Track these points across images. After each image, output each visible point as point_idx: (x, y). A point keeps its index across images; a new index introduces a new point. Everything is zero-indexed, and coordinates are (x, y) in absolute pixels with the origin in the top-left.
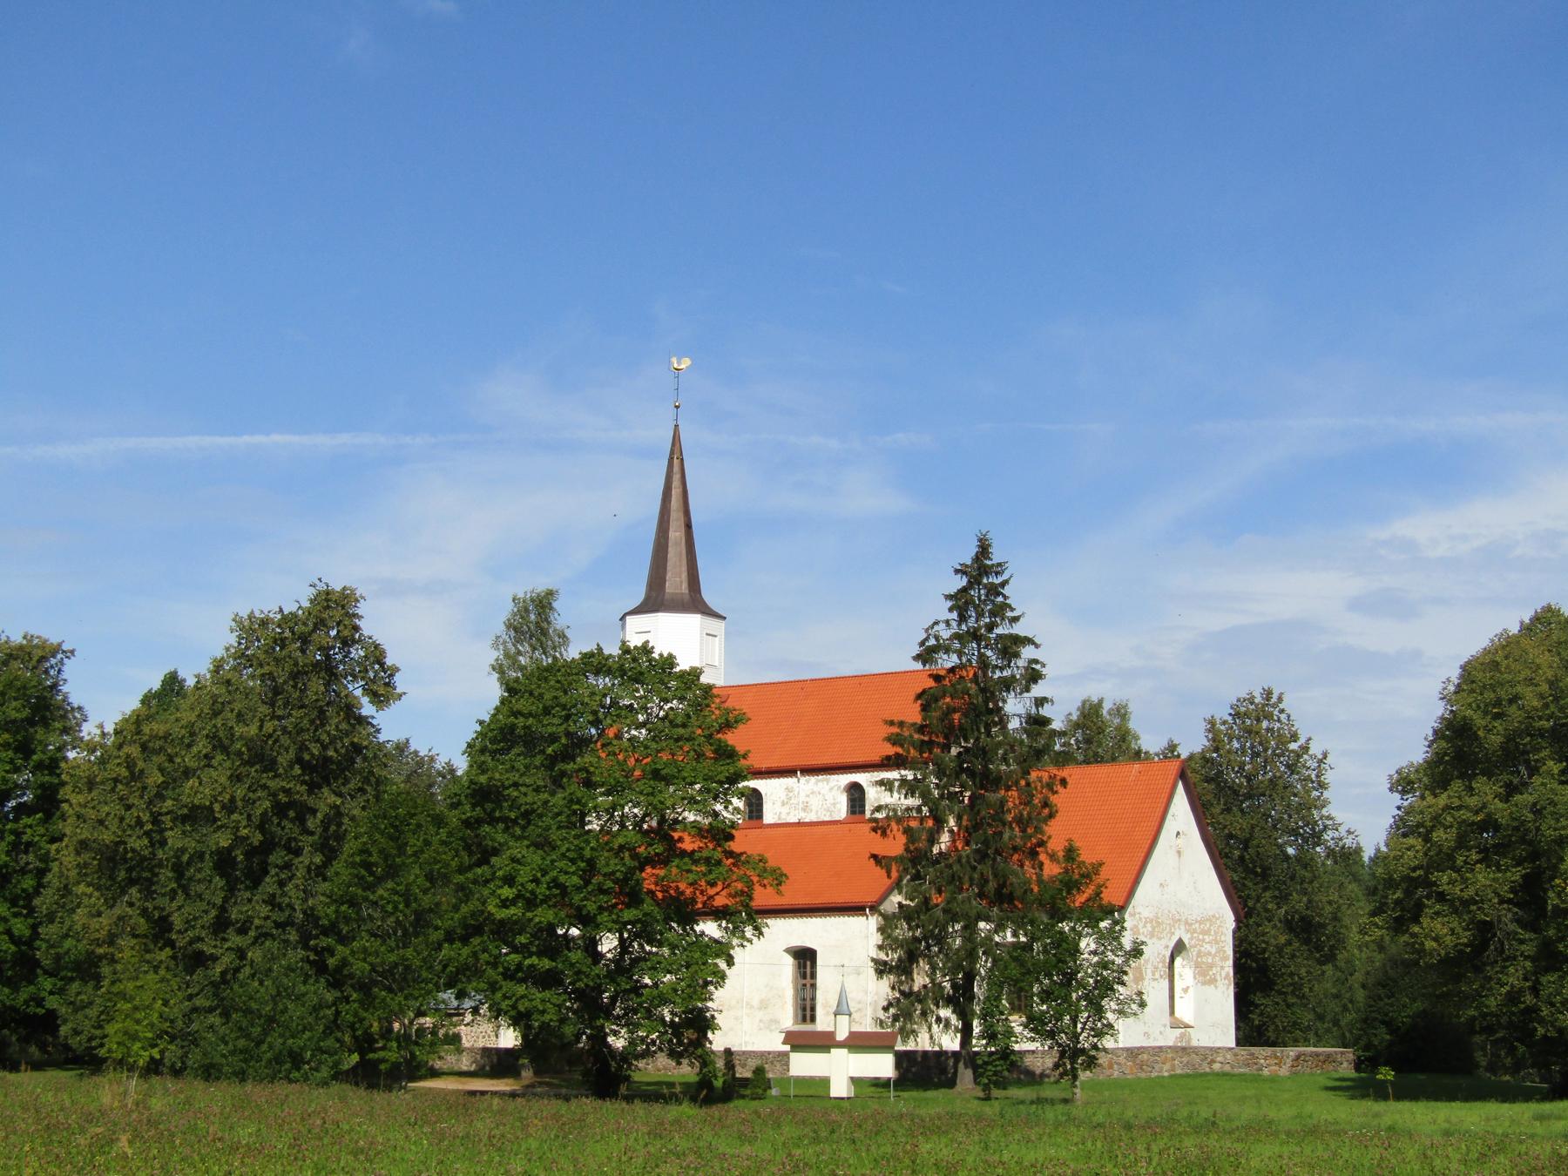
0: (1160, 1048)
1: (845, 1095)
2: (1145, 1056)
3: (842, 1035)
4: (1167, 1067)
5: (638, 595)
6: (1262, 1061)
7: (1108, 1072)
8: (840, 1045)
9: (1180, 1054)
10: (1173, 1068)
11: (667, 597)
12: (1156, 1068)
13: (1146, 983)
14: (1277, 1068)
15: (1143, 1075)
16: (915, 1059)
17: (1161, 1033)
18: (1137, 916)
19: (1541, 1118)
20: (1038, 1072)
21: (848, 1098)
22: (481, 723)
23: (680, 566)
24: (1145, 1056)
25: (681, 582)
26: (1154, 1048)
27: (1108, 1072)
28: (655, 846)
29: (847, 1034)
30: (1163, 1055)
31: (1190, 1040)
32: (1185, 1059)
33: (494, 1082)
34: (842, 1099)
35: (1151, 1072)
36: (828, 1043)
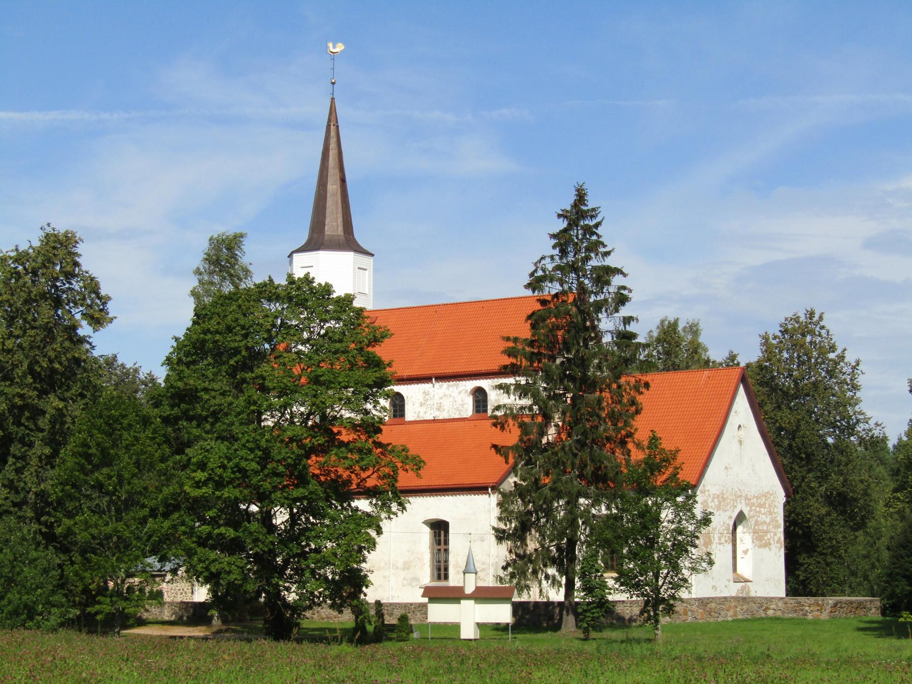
0: (725, 598)
2: (713, 605)
3: (469, 590)
4: (731, 613)
6: (807, 608)
7: (683, 618)
8: (468, 597)
10: (735, 614)
14: (818, 613)
17: (726, 586)
18: (707, 493)
20: (627, 617)
21: (475, 640)
24: (713, 605)
26: (720, 598)
27: (683, 618)
30: (727, 604)
31: (749, 592)
32: (745, 607)
34: (470, 640)
35: (718, 617)
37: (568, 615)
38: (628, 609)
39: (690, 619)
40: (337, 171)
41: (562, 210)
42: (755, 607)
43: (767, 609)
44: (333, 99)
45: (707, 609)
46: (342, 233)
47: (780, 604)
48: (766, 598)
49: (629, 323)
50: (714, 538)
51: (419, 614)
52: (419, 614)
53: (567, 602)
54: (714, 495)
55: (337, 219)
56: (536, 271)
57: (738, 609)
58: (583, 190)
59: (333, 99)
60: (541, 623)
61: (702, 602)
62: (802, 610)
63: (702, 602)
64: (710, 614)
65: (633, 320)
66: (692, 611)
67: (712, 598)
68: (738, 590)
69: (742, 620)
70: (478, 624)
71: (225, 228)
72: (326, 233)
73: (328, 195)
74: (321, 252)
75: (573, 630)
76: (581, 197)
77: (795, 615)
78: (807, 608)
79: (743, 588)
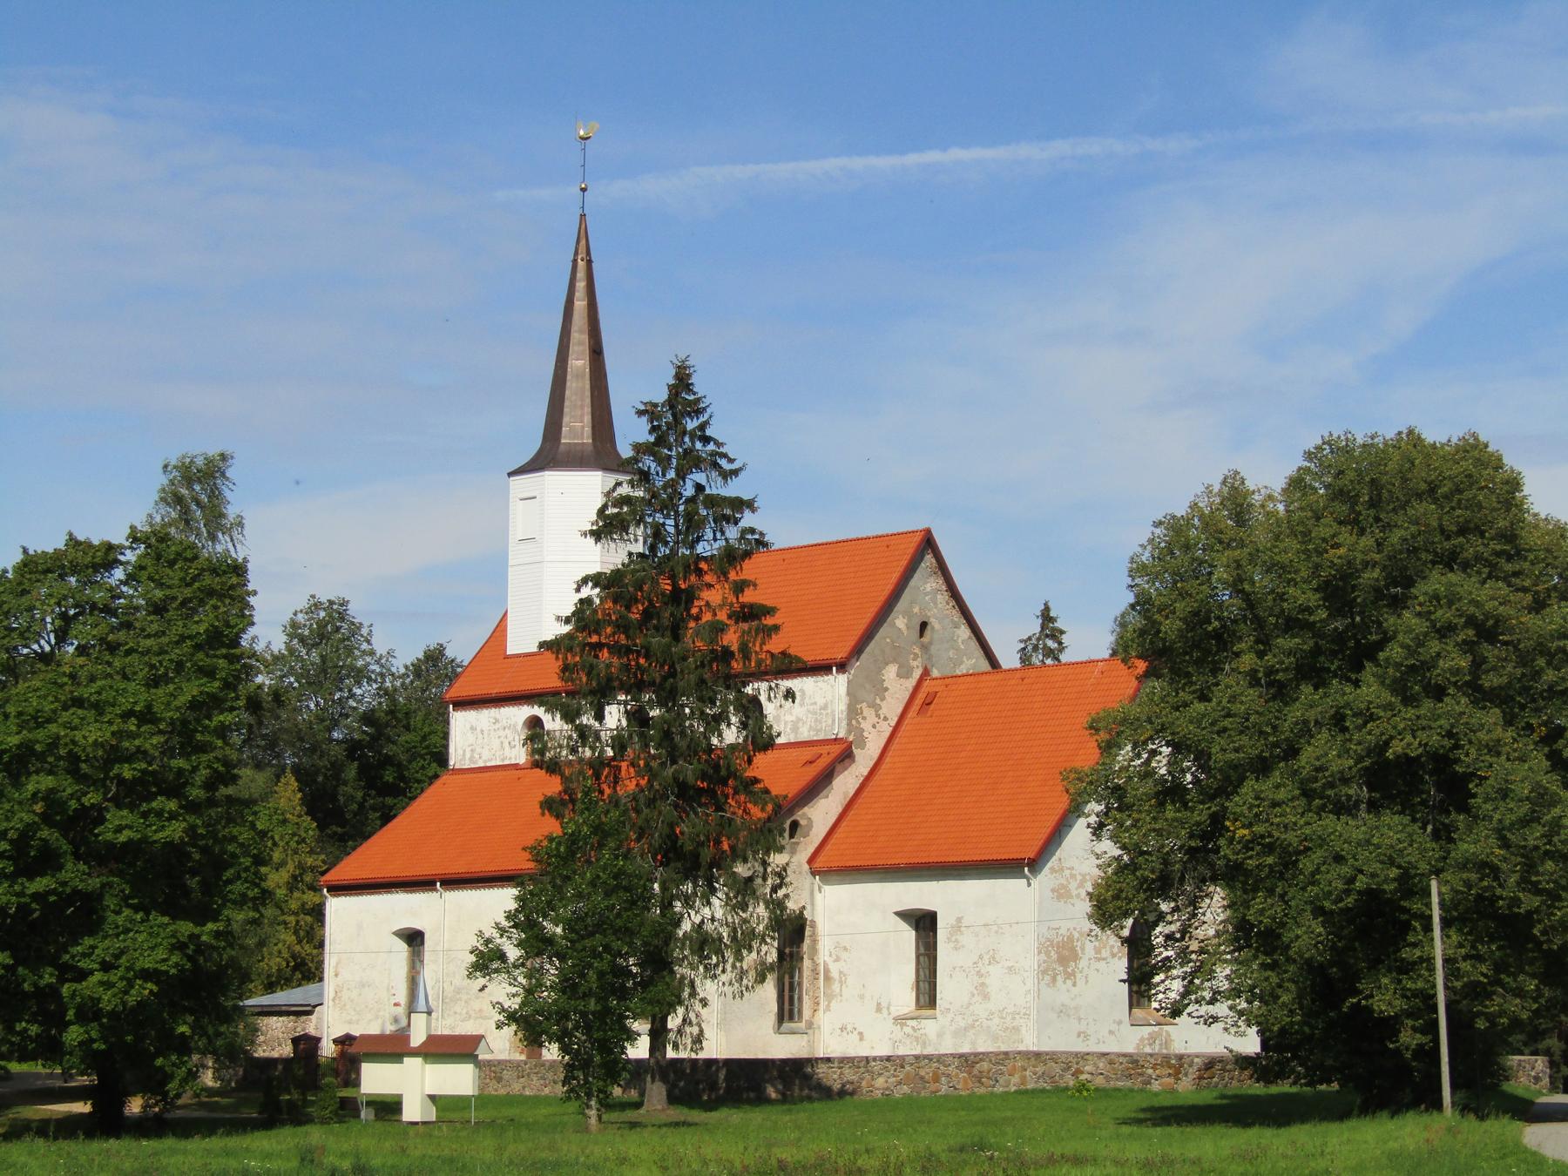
0: (1006, 1053)
1: (419, 1120)
2: (985, 1065)
3: (417, 1038)
4: (1015, 1079)
5: (533, 443)
6: (1150, 1071)
7: (933, 1087)
8: (415, 1053)
9: (1033, 1061)
10: (1023, 1080)
11: (562, 448)
12: (1001, 1081)
13: (1083, 964)
14: (1172, 1080)
15: (982, 1090)
16: (683, 1072)
17: (1111, 1032)
18: (1067, 872)
19: (228, 1153)
20: (837, 1086)
21: (424, 1123)
22: (255, 593)
23: (582, 407)
24: (985, 1065)
25: (583, 427)
26: (997, 1054)
27: (933, 1087)
28: (89, 796)
29: (424, 1038)
30: (1008, 1063)
31: (1167, 1043)
32: (1040, 1070)
33: (1448, 1084)
34: (417, 1123)
35: (994, 1086)
36: (399, 1051)
37: (653, 1081)
38: (835, 1073)
39: (944, 1089)
40: (585, 338)
41: (645, 404)
42: (1057, 1069)
43: (1078, 1072)
44: (583, 216)
45: (975, 1072)
46: (590, 441)
47: (1101, 1065)
48: (1076, 1054)
49: (742, 591)
50: (1083, 949)
51: (535, 1079)
52: (535, 1079)
53: (652, 1061)
54: (1084, 876)
55: (582, 416)
56: (605, 507)
57: (1028, 1073)
58: (685, 368)
59: (583, 216)
60: (701, 1097)
61: (966, 1061)
62: (1141, 1075)
63: (966, 1061)
64: (980, 1082)
65: (749, 586)
66: (948, 1076)
67: (983, 1054)
68: (1142, 1040)
69: (1033, 1091)
70: (432, 1098)
71: (201, 447)
72: (563, 441)
73: (569, 377)
74: (547, 474)
75: (659, 1107)
76: (682, 380)
77: (1129, 1084)
78: (1150, 1071)
79: (1152, 1039)
